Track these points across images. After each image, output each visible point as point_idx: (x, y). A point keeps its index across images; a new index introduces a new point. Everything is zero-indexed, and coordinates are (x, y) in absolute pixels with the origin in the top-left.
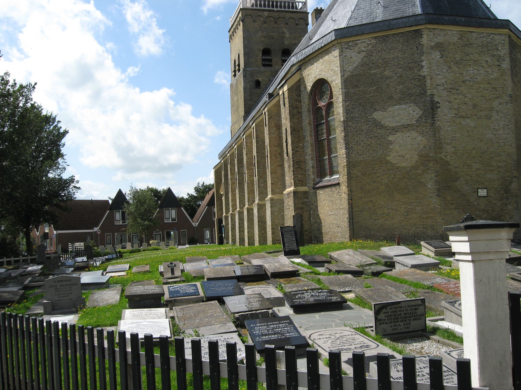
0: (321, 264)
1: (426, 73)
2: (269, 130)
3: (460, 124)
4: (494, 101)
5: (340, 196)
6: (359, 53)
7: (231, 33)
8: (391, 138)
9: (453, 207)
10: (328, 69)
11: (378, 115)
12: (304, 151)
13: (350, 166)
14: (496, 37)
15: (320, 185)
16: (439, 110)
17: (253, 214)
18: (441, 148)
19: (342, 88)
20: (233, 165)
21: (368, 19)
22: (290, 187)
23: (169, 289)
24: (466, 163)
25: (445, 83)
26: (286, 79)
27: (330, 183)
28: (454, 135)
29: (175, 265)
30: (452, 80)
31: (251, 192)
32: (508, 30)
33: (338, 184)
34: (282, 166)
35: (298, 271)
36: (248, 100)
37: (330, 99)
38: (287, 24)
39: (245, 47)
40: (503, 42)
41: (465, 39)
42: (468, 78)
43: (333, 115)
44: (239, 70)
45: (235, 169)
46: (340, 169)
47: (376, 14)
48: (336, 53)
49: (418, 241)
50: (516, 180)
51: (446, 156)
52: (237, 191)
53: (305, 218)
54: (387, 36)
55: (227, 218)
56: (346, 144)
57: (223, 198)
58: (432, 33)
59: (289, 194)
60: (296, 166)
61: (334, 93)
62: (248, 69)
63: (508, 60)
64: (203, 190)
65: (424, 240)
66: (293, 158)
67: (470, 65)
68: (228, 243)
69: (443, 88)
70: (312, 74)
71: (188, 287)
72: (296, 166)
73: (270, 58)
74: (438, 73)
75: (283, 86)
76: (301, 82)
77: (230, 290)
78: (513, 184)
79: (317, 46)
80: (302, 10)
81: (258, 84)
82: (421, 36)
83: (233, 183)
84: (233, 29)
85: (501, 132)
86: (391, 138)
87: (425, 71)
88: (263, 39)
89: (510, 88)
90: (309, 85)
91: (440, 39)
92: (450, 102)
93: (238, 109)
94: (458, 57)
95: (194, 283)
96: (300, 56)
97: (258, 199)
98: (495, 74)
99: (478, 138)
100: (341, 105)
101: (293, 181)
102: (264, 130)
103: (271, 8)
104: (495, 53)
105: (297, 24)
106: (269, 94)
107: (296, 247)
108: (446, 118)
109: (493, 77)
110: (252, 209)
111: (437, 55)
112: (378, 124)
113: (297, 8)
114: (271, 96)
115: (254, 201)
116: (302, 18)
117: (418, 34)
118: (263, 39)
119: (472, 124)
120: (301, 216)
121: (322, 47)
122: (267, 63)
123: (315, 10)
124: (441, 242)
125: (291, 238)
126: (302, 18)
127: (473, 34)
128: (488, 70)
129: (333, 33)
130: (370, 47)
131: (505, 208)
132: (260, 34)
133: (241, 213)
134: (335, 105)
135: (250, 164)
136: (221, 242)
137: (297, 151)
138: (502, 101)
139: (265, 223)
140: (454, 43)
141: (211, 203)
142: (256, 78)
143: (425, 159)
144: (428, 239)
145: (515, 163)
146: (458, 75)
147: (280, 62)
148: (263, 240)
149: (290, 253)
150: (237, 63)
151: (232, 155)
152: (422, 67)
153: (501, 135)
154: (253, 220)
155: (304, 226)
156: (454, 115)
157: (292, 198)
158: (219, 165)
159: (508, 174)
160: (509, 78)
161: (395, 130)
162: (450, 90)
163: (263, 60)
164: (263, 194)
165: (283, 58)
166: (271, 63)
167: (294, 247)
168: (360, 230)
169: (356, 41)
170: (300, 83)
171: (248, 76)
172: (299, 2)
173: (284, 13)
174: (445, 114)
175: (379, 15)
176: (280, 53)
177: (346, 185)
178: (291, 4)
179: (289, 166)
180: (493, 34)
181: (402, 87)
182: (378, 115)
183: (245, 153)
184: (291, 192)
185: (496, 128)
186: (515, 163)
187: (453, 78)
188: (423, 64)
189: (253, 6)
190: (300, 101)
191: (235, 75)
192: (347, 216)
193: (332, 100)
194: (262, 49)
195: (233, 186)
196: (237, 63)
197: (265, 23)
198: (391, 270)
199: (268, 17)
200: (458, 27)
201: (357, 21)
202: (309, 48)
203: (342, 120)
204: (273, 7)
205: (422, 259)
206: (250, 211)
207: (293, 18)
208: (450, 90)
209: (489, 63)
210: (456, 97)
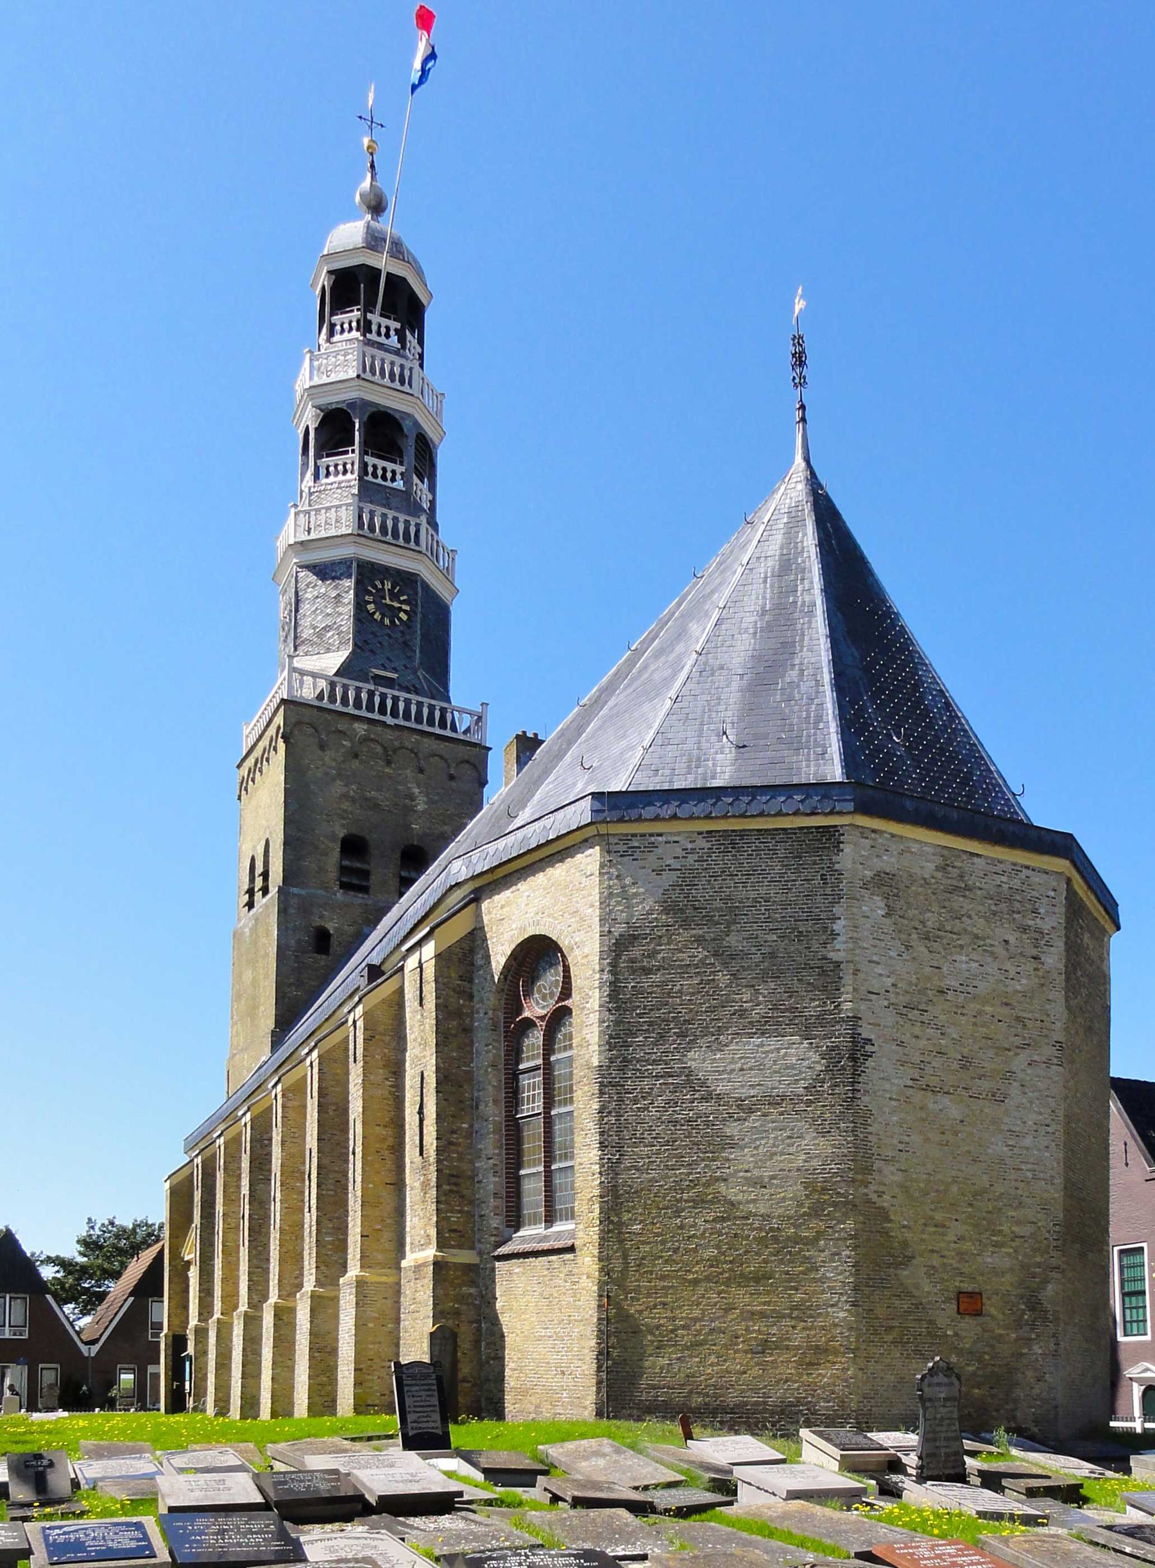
0: (525, 1477)
1: (842, 954)
2: (365, 1075)
3: (921, 1108)
4: (1017, 1054)
5: (575, 1283)
6: (659, 872)
7: (244, 771)
8: (732, 1129)
9: (889, 1338)
10: (566, 905)
11: (698, 1060)
12: (470, 1146)
13: (614, 1201)
14: (1036, 879)
15: (503, 1250)
16: (870, 1063)
17: (292, 1325)
18: (868, 1170)
19: (602, 970)
20: (233, 1174)
21: (691, 778)
22: (423, 1247)
23: (46, 1537)
24: (932, 1218)
25: (891, 989)
26: (430, 921)
27: (545, 1246)
28: (906, 1139)
29: (51, 1464)
30: (910, 984)
31: (292, 1258)
32: (1067, 863)
33: (571, 1249)
34: (399, 1186)
35: (460, 1494)
36: (289, 985)
37: (560, 999)
38: (421, 771)
39: (288, 821)
40: (1052, 894)
41: (955, 872)
42: (955, 984)
43: (571, 1047)
44: (265, 890)
45: (239, 1187)
46: (580, 1206)
47: (714, 765)
48: (590, 859)
49: (792, 1428)
50: (1059, 1276)
51: (880, 1194)
52: (244, 1253)
53: (465, 1343)
54: (743, 834)
55: (201, 1333)
56: (602, 1134)
57: (193, 1274)
58: (867, 843)
59: (418, 1268)
60: (446, 1187)
61: (576, 983)
62: (295, 890)
63: (1060, 944)
64: (109, 1249)
65: (808, 1424)
66: (438, 1161)
67: (961, 947)
68: (199, 1409)
69: (886, 1003)
70: (508, 921)
71: (113, 1529)
72: (446, 1187)
73: (365, 867)
74: (875, 958)
75: (419, 944)
76: (475, 940)
77: (258, 1545)
78: (1050, 1287)
79: (535, 835)
80: (467, 738)
81: (322, 940)
82: (837, 846)
83: (232, 1229)
84: (250, 762)
85: (1028, 1141)
86: (732, 1129)
87: (839, 950)
88: (346, 805)
89: (1059, 1024)
90: (499, 954)
91: (888, 862)
92: (901, 1044)
93: (255, 1007)
94: (932, 920)
95: (135, 1520)
96: (481, 861)
97: (313, 1278)
98: (1024, 981)
99: (969, 1152)
100: (594, 1018)
101: (433, 1232)
102: (347, 1073)
103: (376, 716)
104: (1031, 923)
105: (452, 778)
106: (370, 966)
107: (439, 1424)
108: (887, 1086)
109: (1019, 988)
110: (292, 1311)
111: (874, 907)
112: (690, 1080)
113: (454, 728)
114: (375, 972)
115: (301, 1286)
116: (467, 762)
117: (830, 838)
118: (346, 805)
119: (955, 1112)
120: (454, 1336)
121: (549, 842)
122: (355, 880)
123: (518, 737)
124: (857, 1433)
125: (426, 1398)
126: (467, 762)
127: (976, 860)
128: (1007, 965)
129: (587, 803)
130: (691, 859)
131: (1025, 1351)
132: (338, 788)
133: (252, 1322)
134: (576, 1019)
135: (294, 1173)
136: (177, 1404)
137: (450, 1143)
138: (1036, 1058)
139: (334, 1351)
140: (925, 879)
141: (149, 1286)
142: (317, 922)
143: (821, 1199)
144: (826, 1422)
145: (1057, 1228)
146: (928, 969)
147: (394, 883)
148: (323, 1401)
149: (425, 1441)
150: (259, 869)
151: (234, 1145)
152: (834, 935)
153: (1027, 1148)
154: (293, 1343)
155: (460, 1365)
156: (910, 1083)
157: (428, 1282)
158: (186, 1172)
159: (1038, 1259)
160: (1057, 995)
161: (746, 1108)
162: (904, 1011)
163: (343, 870)
164: (332, 1262)
165: (404, 874)
166: (364, 883)
167: (433, 1423)
168: (623, 1392)
169: (651, 835)
170: (473, 941)
171: (292, 911)
172: (462, 711)
173: (415, 737)
174: (885, 1076)
175: (723, 770)
176: (398, 855)
177: (596, 1252)
178: (437, 714)
179: (425, 1186)
180: (1027, 867)
181: (772, 986)
182: (698, 1060)
183: (277, 1137)
184: (424, 1264)
185: (1017, 1129)
186: (1057, 1228)
187: (914, 979)
188: (838, 926)
189: (320, 697)
190: (471, 997)
191: (250, 905)
192: (593, 1343)
193: (566, 1003)
194: (342, 835)
195: (231, 1236)
196: (259, 869)
197: (356, 756)
198: (730, 1503)
199: (366, 739)
200: (939, 834)
201: (658, 779)
202: (510, 839)
203: (596, 1064)
204: (382, 711)
205: (814, 1478)
206: (285, 1317)
207: (441, 757)
208: (904, 1011)
209: (1012, 949)
210: (917, 1030)
